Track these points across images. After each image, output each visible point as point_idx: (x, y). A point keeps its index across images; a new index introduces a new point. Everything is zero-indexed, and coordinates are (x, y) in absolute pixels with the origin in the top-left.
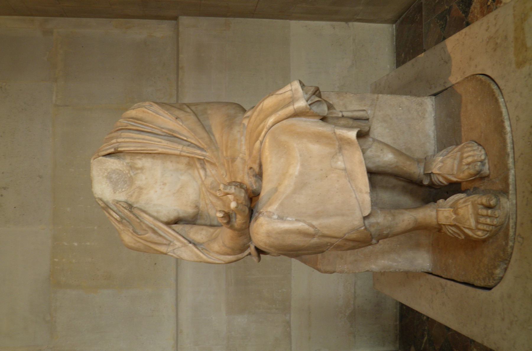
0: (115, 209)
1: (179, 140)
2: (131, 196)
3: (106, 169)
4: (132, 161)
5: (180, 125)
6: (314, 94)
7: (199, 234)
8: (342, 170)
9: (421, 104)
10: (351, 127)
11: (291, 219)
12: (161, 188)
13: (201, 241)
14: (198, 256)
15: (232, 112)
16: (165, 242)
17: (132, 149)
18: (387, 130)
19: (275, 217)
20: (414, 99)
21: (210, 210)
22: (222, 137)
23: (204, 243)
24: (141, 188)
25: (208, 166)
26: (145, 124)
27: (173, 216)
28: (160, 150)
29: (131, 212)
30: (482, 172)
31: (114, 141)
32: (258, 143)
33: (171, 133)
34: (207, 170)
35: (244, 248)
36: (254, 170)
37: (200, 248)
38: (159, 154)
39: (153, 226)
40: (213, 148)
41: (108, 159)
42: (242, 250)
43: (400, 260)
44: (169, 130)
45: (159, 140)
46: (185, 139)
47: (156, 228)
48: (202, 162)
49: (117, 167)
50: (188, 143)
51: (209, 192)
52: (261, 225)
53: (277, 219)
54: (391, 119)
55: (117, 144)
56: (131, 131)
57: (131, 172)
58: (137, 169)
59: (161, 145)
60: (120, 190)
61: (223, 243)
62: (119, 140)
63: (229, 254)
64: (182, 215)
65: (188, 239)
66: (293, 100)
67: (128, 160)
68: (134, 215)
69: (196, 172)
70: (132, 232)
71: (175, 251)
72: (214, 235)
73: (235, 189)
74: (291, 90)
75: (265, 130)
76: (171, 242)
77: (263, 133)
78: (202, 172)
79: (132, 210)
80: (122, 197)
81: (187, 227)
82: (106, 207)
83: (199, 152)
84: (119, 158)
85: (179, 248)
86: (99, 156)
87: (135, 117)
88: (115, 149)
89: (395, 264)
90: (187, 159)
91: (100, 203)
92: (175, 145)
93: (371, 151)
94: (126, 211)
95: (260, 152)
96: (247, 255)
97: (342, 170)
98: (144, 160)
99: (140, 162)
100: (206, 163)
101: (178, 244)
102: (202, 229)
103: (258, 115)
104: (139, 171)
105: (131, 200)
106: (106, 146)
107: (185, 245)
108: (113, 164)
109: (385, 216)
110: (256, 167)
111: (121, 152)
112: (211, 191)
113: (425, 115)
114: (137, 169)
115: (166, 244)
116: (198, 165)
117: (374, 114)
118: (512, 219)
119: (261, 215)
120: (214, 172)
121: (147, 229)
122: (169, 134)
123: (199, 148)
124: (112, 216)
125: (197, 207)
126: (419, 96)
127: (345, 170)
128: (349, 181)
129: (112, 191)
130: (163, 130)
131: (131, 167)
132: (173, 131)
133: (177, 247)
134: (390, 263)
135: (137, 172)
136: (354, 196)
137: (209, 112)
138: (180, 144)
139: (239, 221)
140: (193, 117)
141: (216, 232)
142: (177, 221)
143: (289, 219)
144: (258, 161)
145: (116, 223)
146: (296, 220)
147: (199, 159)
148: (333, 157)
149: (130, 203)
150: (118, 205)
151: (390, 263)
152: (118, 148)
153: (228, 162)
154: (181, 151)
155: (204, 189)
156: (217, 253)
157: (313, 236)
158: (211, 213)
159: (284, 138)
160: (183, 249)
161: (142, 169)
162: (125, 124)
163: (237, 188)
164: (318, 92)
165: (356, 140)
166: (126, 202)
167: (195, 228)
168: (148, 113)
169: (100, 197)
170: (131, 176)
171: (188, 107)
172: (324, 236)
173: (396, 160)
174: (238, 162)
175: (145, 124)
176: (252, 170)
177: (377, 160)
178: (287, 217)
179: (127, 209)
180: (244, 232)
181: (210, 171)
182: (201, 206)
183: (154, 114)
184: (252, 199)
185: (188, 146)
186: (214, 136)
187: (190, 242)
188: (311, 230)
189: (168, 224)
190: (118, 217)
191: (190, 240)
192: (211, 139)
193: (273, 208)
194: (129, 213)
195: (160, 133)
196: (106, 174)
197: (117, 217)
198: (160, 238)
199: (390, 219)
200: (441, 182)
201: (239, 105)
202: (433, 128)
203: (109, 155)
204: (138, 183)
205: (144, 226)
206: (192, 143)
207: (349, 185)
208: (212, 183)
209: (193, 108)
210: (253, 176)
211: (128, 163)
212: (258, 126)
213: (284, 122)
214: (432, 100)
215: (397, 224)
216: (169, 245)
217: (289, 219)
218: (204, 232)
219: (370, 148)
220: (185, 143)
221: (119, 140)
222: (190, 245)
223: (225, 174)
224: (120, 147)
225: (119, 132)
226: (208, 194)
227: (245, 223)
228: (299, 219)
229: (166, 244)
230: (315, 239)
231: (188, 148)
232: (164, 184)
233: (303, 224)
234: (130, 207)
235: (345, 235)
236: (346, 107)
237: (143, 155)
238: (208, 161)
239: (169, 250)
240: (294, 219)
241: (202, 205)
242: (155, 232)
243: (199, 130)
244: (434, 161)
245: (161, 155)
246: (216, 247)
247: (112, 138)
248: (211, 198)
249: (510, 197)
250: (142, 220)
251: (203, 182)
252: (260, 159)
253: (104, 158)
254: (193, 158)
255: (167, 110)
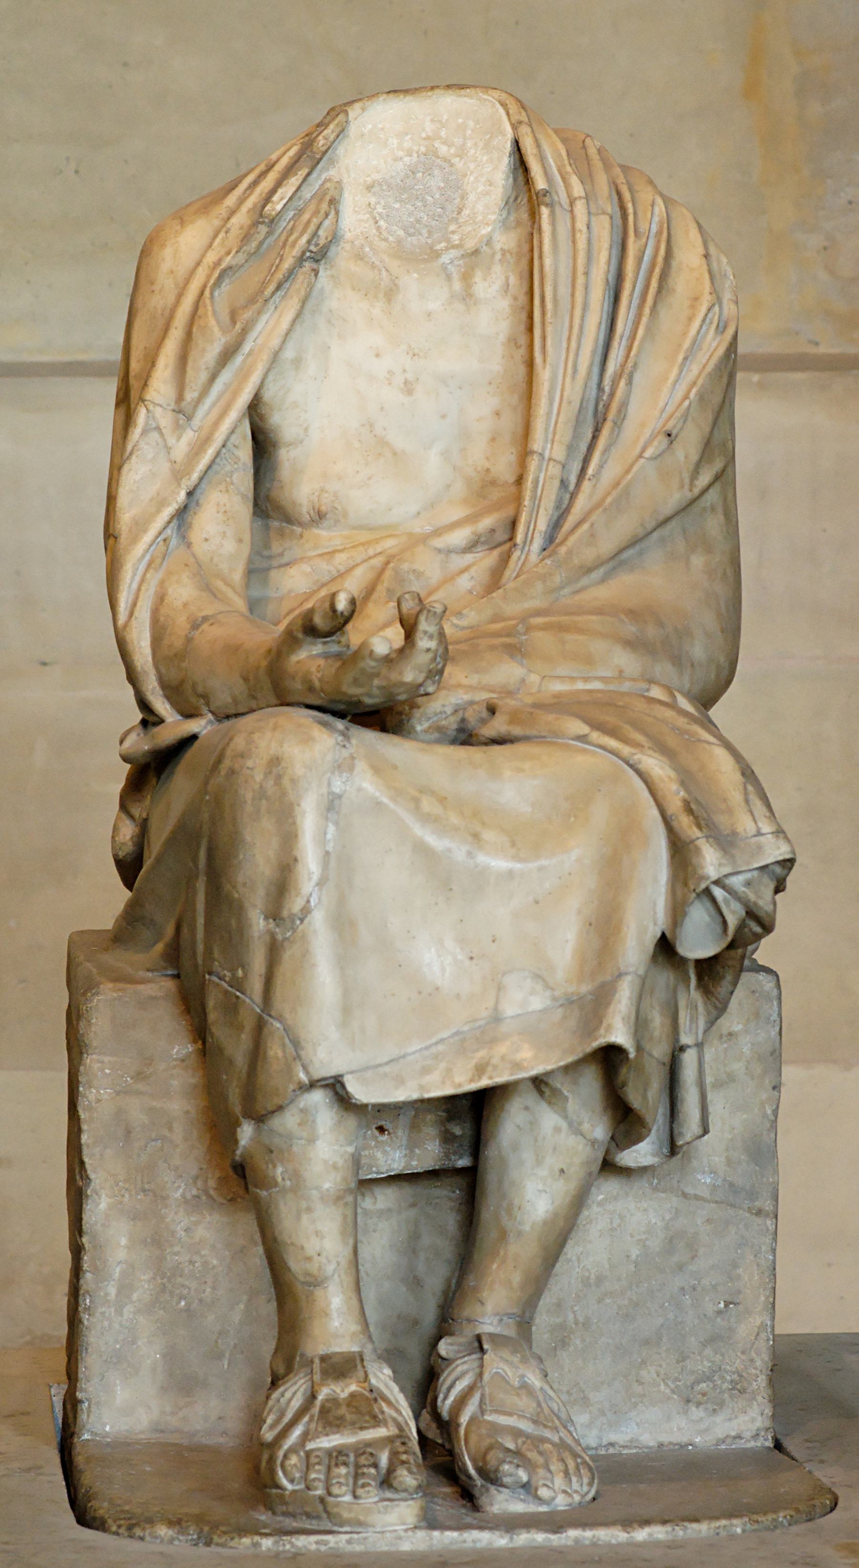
0: (307, 193)
1: (583, 447)
2: (360, 257)
3: (462, 153)
4: (498, 256)
5: (643, 450)
6: (751, 914)
7: (222, 527)
8: (496, 1009)
9: (742, 1391)
10: (640, 1025)
11: (329, 836)
12: (390, 372)
13: (196, 536)
14: (140, 525)
15: (698, 651)
16: (190, 395)
17: (548, 262)
18: (635, 1252)
19: (338, 786)
20: (759, 1363)
21: (306, 568)
22: (599, 611)
23: (189, 545)
24: (390, 293)
25: (488, 560)
26: (647, 311)
27: (284, 423)
28: (544, 375)
29: (301, 260)
30: (492, 1488)
31: (578, 190)
32: (579, 727)
33: (611, 415)
34: (469, 558)
35: (186, 698)
36: (483, 722)
37: (169, 531)
38: (530, 364)
39: (247, 347)
40: (557, 579)
41: (505, 161)
42: (174, 691)
43: (128, 1311)
44: (624, 405)
45: (583, 369)
46: (590, 471)
47: (239, 359)
48: (501, 536)
49: (472, 197)
50: (573, 479)
51: (387, 563)
52: (308, 740)
53: (330, 793)
54: (681, 1267)
55: (565, 201)
56: (615, 252)
57: (453, 253)
58: (467, 278)
59: (563, 384)
60: (380, 209)
61: (205, 619)
62: (580, 208)
63: (156, 641)
64: (285, 456)
65: (203, 485)
66: (726, 842)
67: (506, 241)
68: (290, 274)
69: (458, 513)
70: (224, 265)
71: (155, 435)
72: (219, 584)
73: (428, 650)
74: (759, 834)
75: (626, 750)
76: (189, 418)
77: (613, 743)
78: (460, 537)
79: (307, 265)
80: (353, 219)
81: (244, 479)
82: (310, 154)
83: (542, 525)
84: (510, 203)
85: (168, 449)
86: (515, 127)
87: (674, 264)
88: (546, 193)
89: (112, 1291)
90: (510, 477)
91: (330, 132)
92: (564, 434)
93: (557, 1130)
94: (304, 239)
95: (548, 739)
96: (144, 705)
97: (496, 1009)
98: (504, 304)
99: (495, 289)
100: (496, 553)
101: (181, 447)
102: (240, 541)
103: (674, 728)
104: (457, 286)
105: (341, 256)
106: (556, 152)
107: (178, 475)
108: (487, 182)
109: (335, 1167)
110: (498, 726)
111: (534, 215)
112: (388, 573)
113: (698, 1404)
114: (467, 278)
115: (180, 398)
116: (487, 523)
117: (697, 1198)
118: (349, 1542)
119: (340, 738)
120: (464, 583)
121: (238, 326)
122: (607, 407)
123: (556, 525)
124: (279, 184)
125: (320, 516)
126: (771, 1382)
127: (497, 1018)
128: (457, 1033)
129: (376, 176)
130: (622, 383)
131: (476, 252)
132: (618, 424)
133: (171, 441)
134: (117, 1272)
135: (456, 276)
136: (410, 1050)
137: (698, 561)
138: (571, 449)
139: (310, 659)
140: (675, 498)
141: (230, 594)
142: (263, 445)
143: (331, 829)
144: (517, 731)
145: (253, 199)
146: (327, 853)
147: (514, 524)
148: (538, 977)
149: (332, 252)
150: (324, 206)
151: (117, 1272)
152: (551, 206)
153: (509, 635)
154: (541, 455)
155: (390, 543)
156: (161, 598)
157: (275, 914)
158: (293, 571)
159: (600, 813)
160: (165, 467)
161: (467, 296)
162: (643, 227)
163: (430, 655)
164: (758, 929)
165: (596, 1044)
166: (335, 238)
167: (244, 510)
168: (690, 319)
169: (353, 129)
170: (437, 255)
171: (717, 478)
172: (274, 950)
173: (527, 1228)
174: (508, 672)
175: (647, 311)
176: (485, 714)
177: (528, 1156)
178: (336, 824)
179: (309, 242)
180: (273, 687)
181: (467, 569)
182: (323, 533)
183: (687, 344)
184: (382, 716)
185: (563, 483)
186: (603, 580)
187: (190, 494)
188: (295, 905)
189: (255, 410)
190: (279, 207)
191: (198, 491)
192: (589, 570)
193: (365, 784)
194: (296, 252)
195: (612, 367)
196: (443, 150)
197: (277, 204)
198: (204, 376)
199: (327, 1185)
200: (444, 1380)
201: (729, 682)
202: (648, 1439)
203: (521, 165)
204: (410, 282)
205: (247, 315)
206: (573, 496)
207: (445, 1034)
208: (418, 574)
209: (713, 496)
210: (463, 720)
211: (489, 242)
212: (637, 725)
213: (655, 812)
214: (756, 1436)
215: (309, 1210)
216: (179, 411)
217: (331, 829)
218: (229, 546)
219: (570, 1124)
220: (576, 467)
221: (580, 208)
222: (182, 495)
223: (464, 623)
224: (552, 214)
225: (611, 207)
226: (377, 562)
227: (311, 689)
228: (333, 864)
229: (180, 398)
230: (262, 923)
231: (557, 483)
232: (408, 388)
233: (315, 878)
234: (318, 256)
235: (280, 1019)
236: (719, 1085)
237: (523, 299)
238: (505, 560)
239: (158, 411)
240: (330, 847)
241: (326, 536)
242: (226, 356)
243: (625, 526)
244: (524, 1360)
245: (522, 370)
246: (183, 592)
247: (587, 178)
248: (358, 572)
249: (421, 1534)
250: (271, 306)
251: (424, 539)
252: (526, 739)
253: (508, 146)
254: (518, 499)
255: (702, 398)
